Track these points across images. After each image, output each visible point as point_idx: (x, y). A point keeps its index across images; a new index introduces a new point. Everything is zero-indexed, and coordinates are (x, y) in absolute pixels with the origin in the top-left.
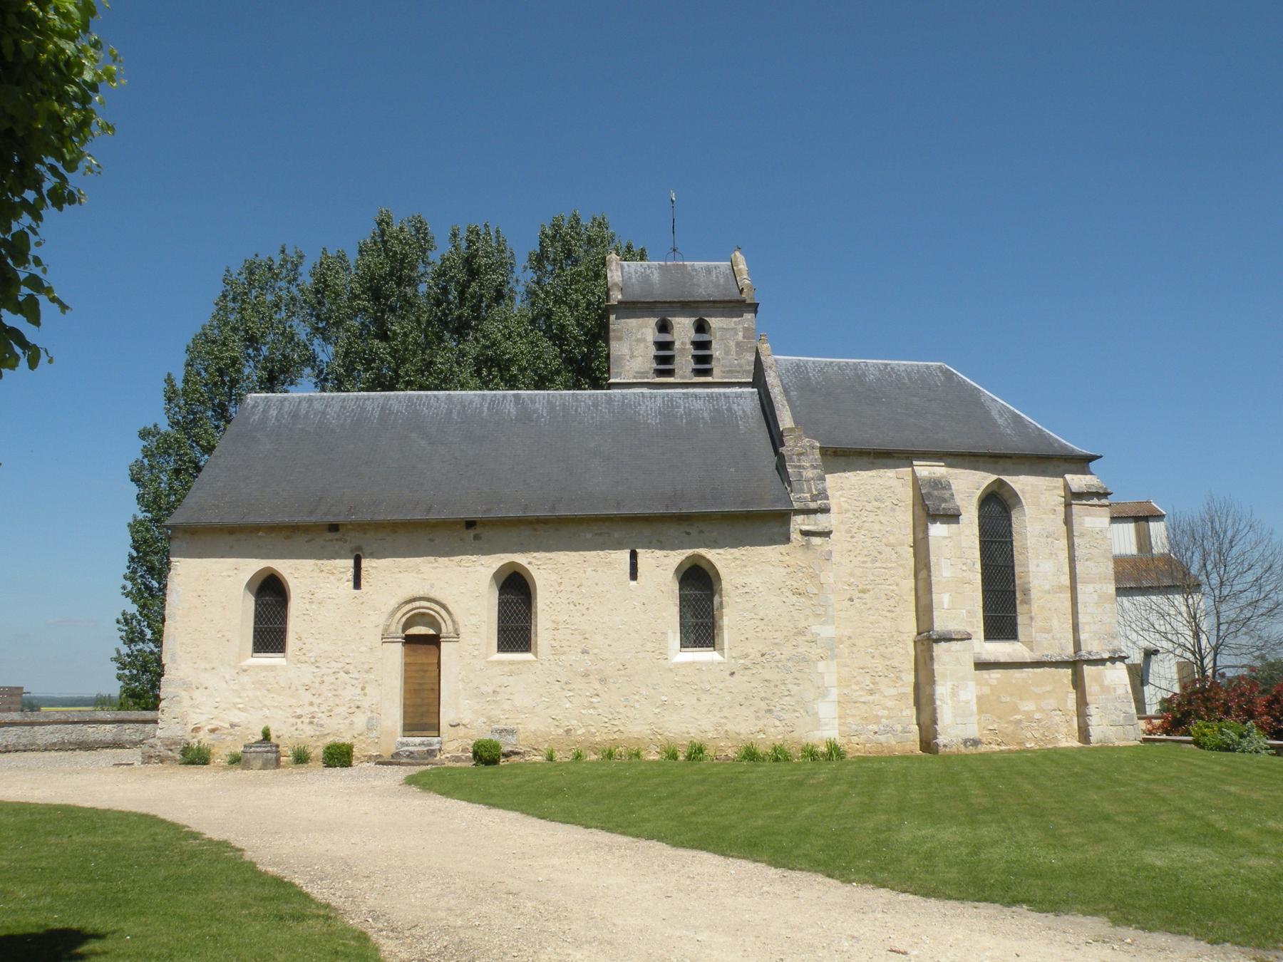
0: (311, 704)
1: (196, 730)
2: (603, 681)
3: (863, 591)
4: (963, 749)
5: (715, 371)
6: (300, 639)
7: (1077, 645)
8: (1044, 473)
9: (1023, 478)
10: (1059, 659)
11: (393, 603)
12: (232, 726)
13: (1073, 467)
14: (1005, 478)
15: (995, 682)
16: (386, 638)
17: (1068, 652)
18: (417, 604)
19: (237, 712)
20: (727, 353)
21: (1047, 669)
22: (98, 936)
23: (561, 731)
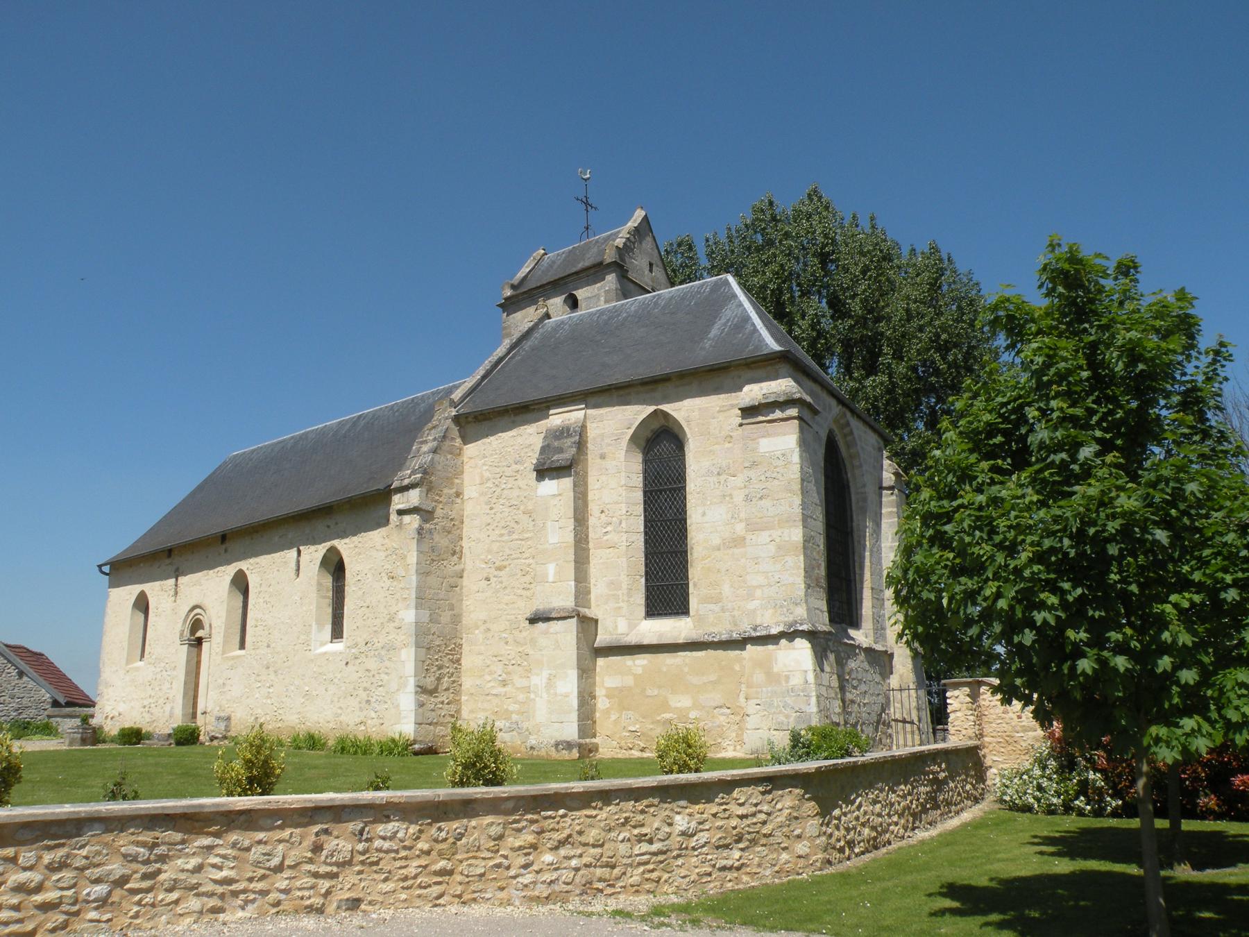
3: (499, 569)
4: (554, 754)
8: (717, 390)
9: (688, 403)
10: (724, 637)
13: (760, 373)
14: (666, 407)
15: (640, 671)
21: (711, 652)
22: (942, 912)
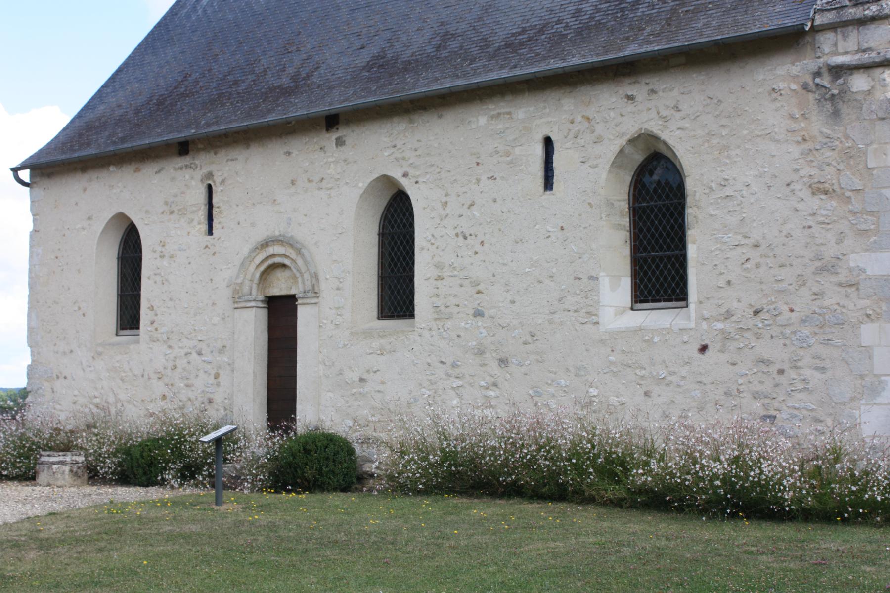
16: (238, 300)
18: (271, 250)
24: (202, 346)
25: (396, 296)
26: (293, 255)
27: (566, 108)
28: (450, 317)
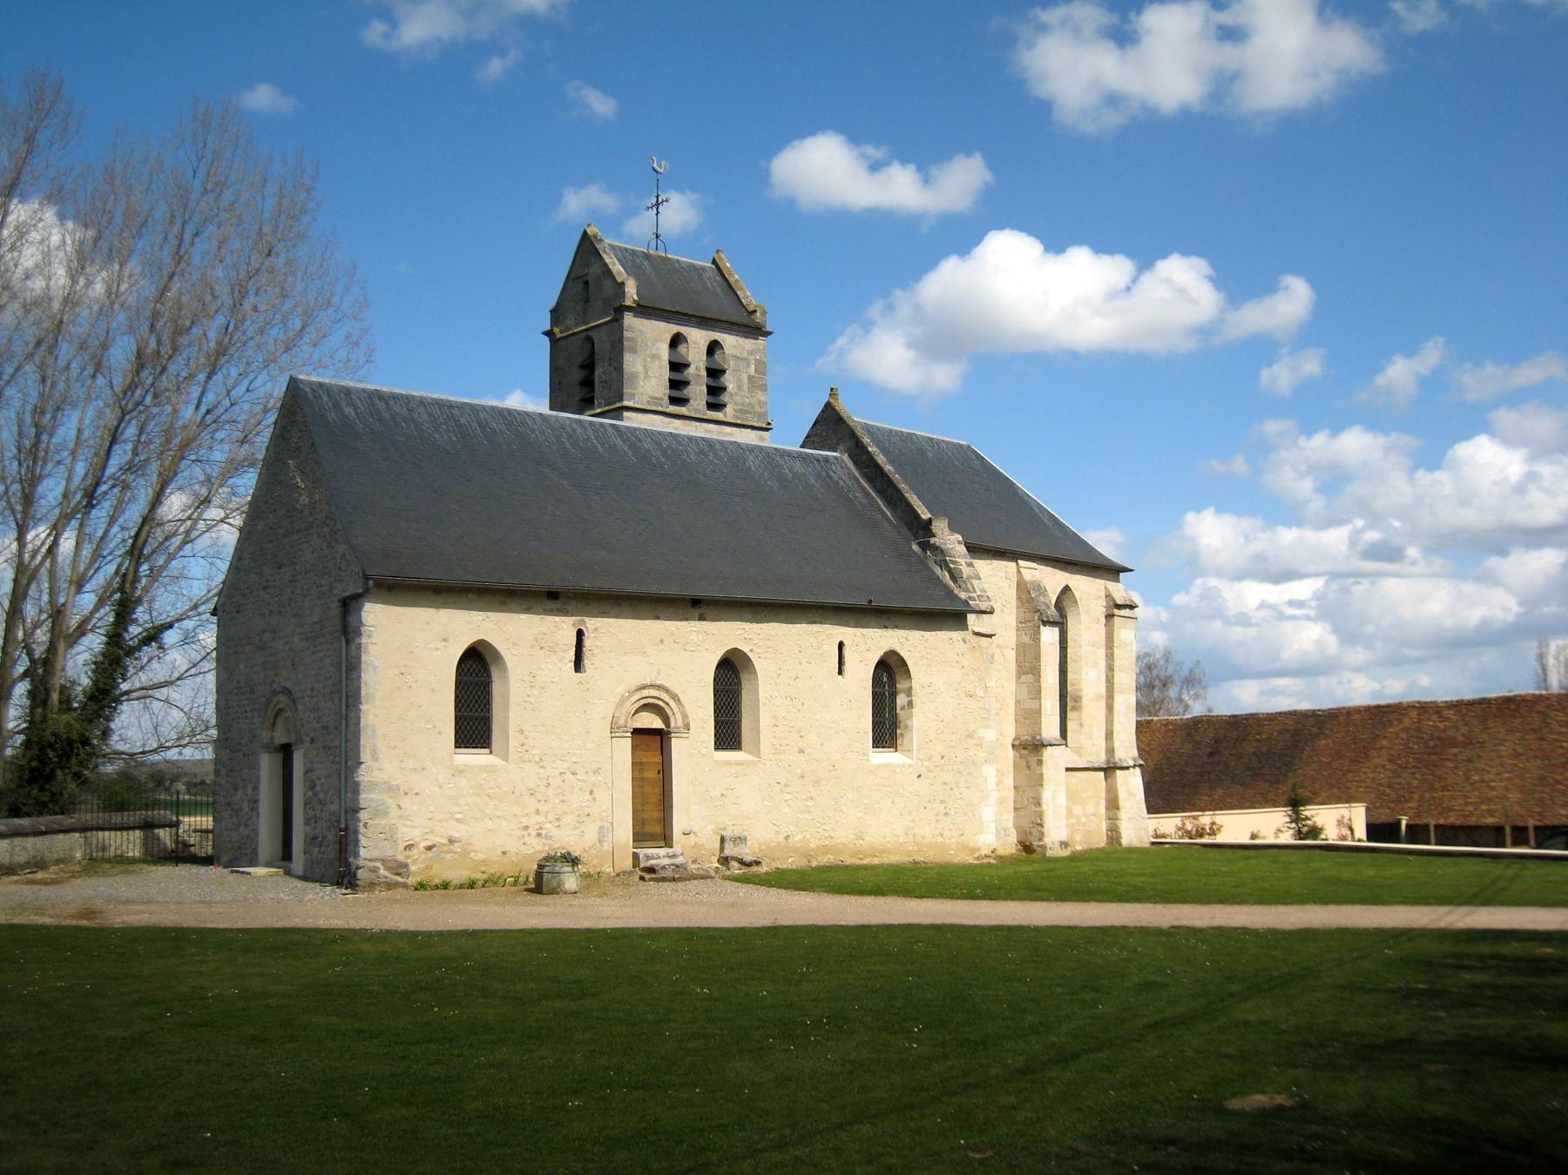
0: (538, 812)
1: (409, 847)
2: (817, 783)
5: (729, 409)
6: (521, 732)
7: (1110, 751)
11: (620, 690)
12: (451, 841)
16: (614, 728)
17: (1100, 759)
18: (646, 692)
19: (455, 824)
20: (740, 388)
23: (781, 838)
24: (578, 768)
25: (728, 734)
26: (667, 698)
27: (640, 368)
28: (783, 752)
